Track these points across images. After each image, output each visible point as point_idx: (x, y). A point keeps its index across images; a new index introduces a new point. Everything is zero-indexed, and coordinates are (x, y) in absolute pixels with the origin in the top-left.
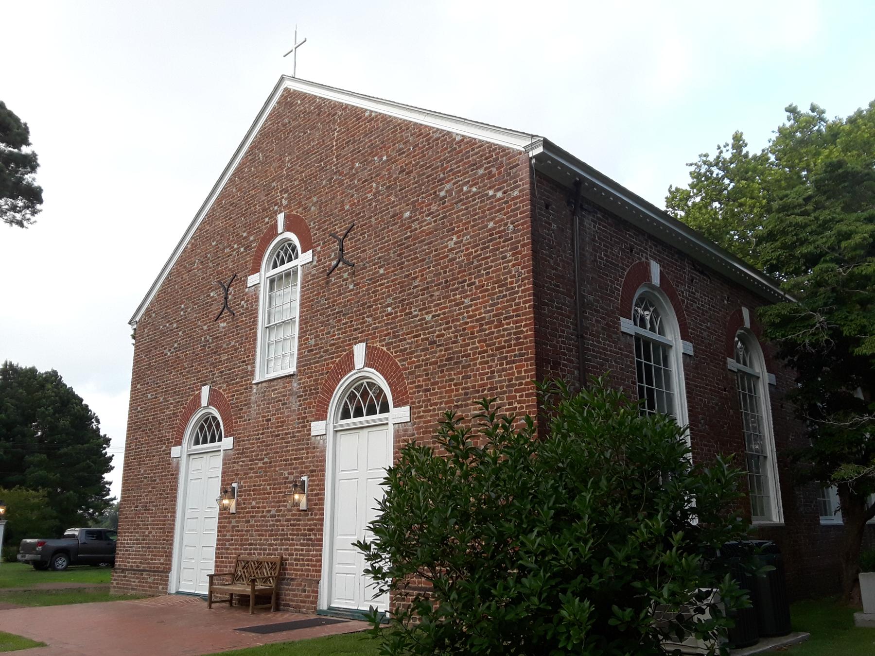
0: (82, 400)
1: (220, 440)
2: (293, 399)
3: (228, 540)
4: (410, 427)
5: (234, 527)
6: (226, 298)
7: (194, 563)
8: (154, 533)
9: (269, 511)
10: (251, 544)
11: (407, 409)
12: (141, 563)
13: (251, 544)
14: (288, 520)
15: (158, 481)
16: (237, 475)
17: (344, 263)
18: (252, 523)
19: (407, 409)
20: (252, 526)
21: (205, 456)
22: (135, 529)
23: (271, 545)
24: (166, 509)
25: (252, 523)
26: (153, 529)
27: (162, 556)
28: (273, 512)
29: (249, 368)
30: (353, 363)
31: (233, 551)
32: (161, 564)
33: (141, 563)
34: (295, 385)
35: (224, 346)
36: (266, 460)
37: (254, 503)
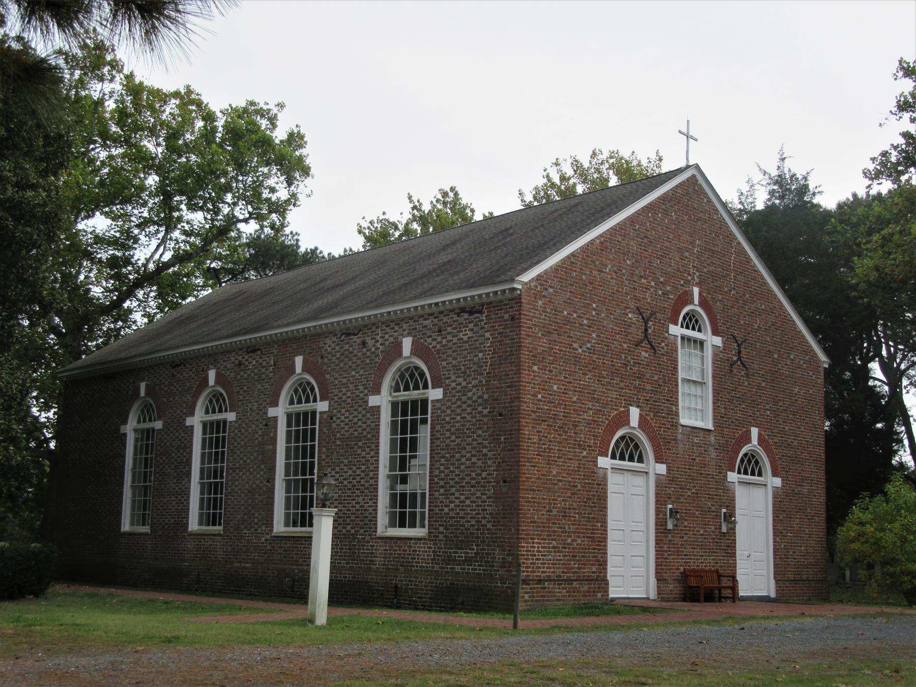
0: (693, 190)
1: (315, 401)
2: (711, 449)
3: (666, 551)
4: (780, 491)
5: (670, 540)
6: (646, 330)
7: (631, 570)
8: (579, 541)
9: (698, 531)
10: (686, 555)
11: (327, 402)
12: (563, 572)
13: (686, 555)
14: (713, 539)
15: (579, 487)
16: (669, 498)
17: (742, 363)
18: (686, 538)
19: (327, 402)
20: (685, 541)
21: (626, 473)
22: (548, 535)
23: (702, 556)
24: (593, 518)
25: (686, 538)
26: (578, 537)
27: (593, 565)
28: (702, 531)
29: (674, 408)
30: (750, 438)
31: (678, 566)
32: (593, 572)
33: (563, 572)
34: (713, 438)
35: (648, 376)
36: (693, 491)
37: (686, 523)
